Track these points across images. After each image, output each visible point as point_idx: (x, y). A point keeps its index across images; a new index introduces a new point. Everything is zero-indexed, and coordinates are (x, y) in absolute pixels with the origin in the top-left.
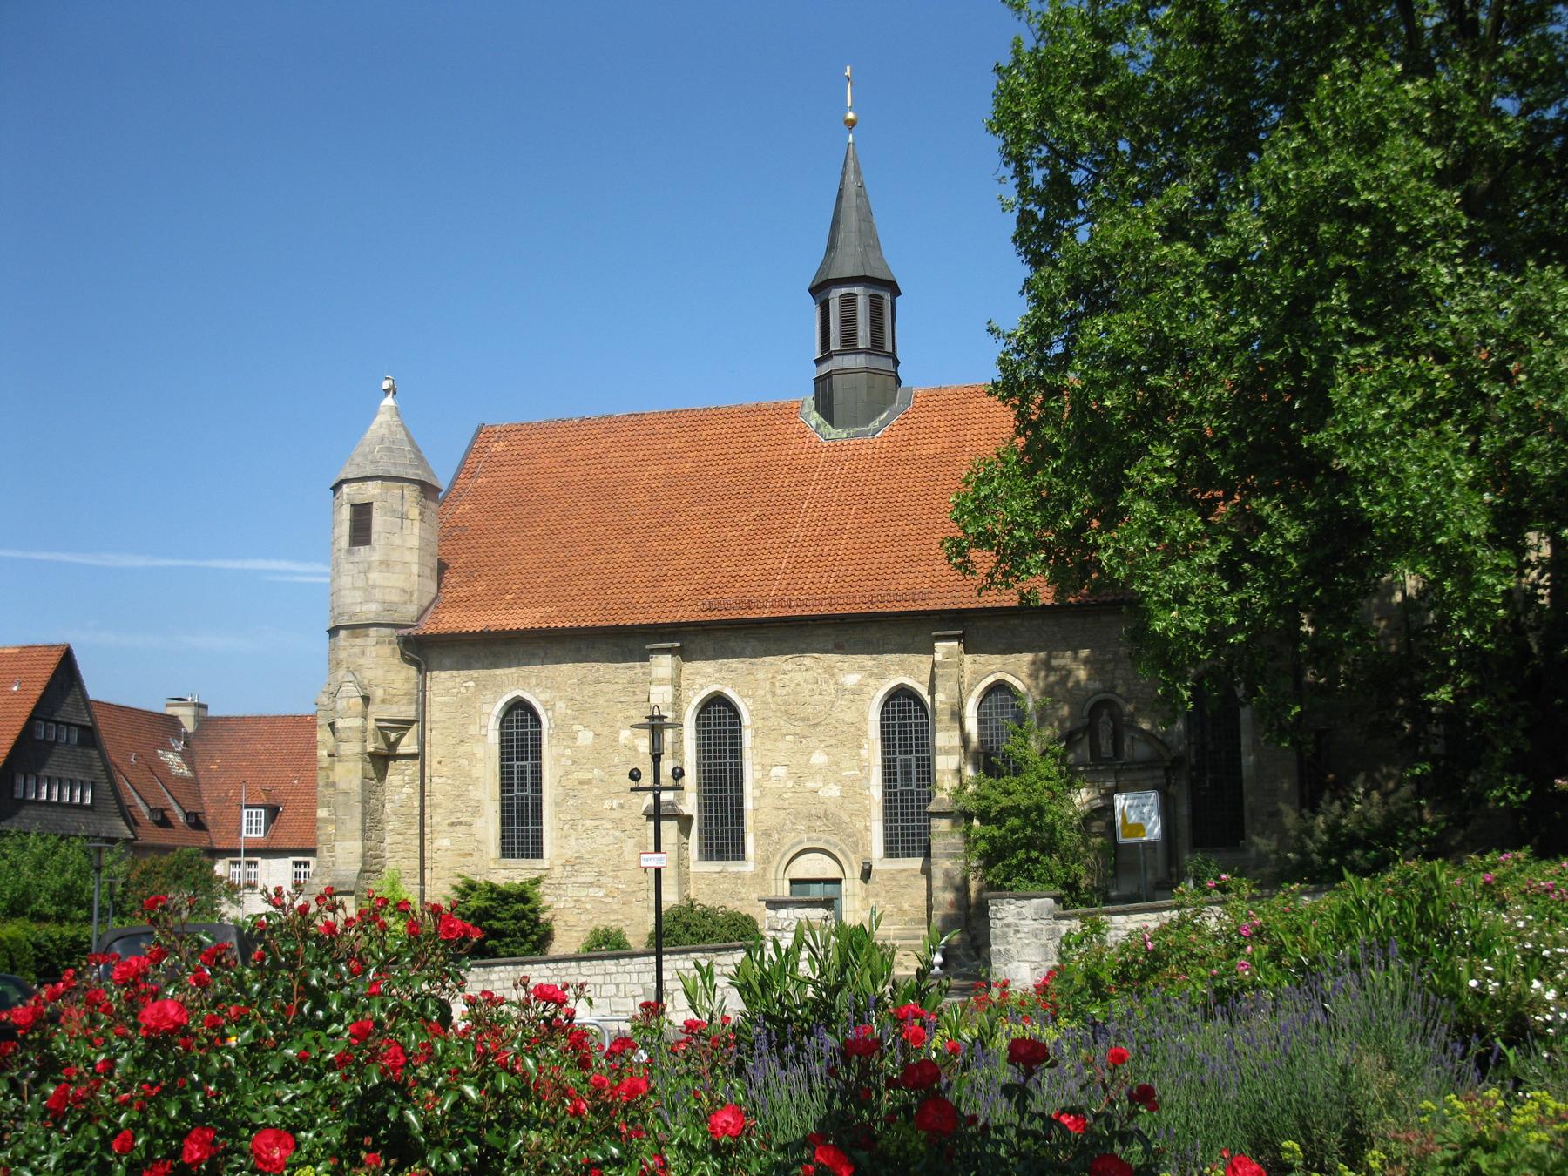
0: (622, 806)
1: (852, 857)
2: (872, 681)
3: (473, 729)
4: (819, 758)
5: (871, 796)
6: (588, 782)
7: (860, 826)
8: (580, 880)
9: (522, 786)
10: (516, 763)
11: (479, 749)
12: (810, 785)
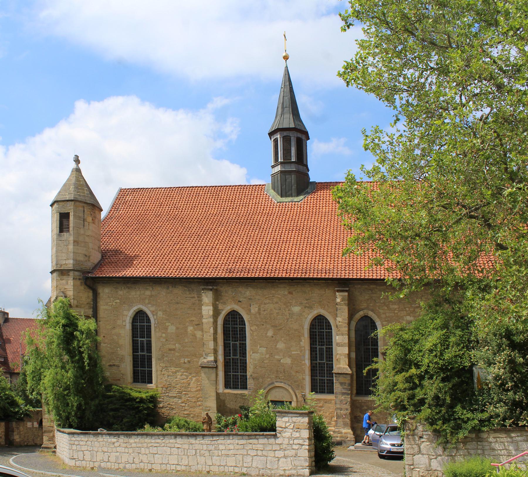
0: (189, 362)
1: (297, 391)
2: (306, 310)
3: (119, 322)
4: (281, 345)
5: (305, 364)
6: (174, 350)
7: (300, 377)
8: (170, 395)
9: (142, 350)
10: (140, 339)
11: (122, 332)
12: (276, 357)
